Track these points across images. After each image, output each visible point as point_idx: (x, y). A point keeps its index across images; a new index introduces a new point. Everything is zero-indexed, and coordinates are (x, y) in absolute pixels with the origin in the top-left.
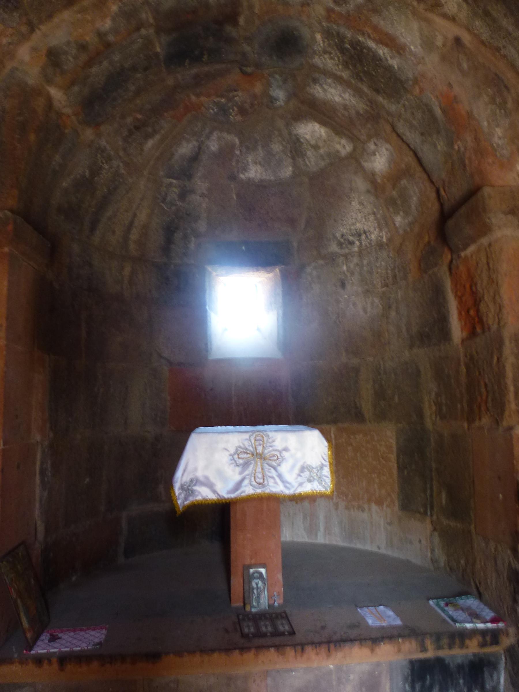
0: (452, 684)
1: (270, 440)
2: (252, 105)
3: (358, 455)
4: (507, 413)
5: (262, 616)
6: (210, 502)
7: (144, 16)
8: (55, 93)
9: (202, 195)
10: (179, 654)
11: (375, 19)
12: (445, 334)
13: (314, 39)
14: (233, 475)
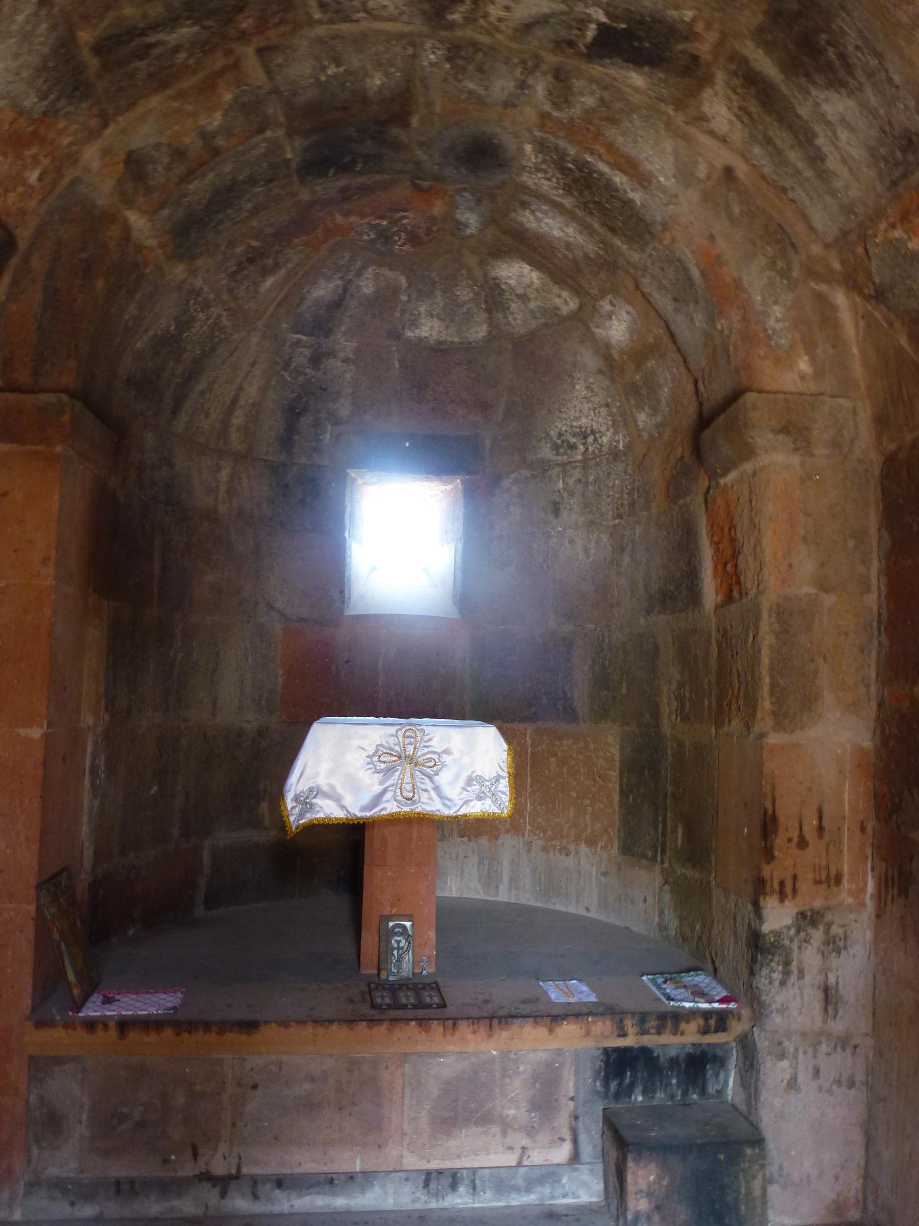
0: (661, 1084)
1: (426, 738)
2: (428, 232)
4: (759, 714)
5: (404, 985)
6: (336, 822)
7: (270, 111)
8: (136, 220)
9: (346, 361)
10: (284, 1024)
11: (611, 133)
12: (694, 597)
13: (521, 150)
14: (372, 784)
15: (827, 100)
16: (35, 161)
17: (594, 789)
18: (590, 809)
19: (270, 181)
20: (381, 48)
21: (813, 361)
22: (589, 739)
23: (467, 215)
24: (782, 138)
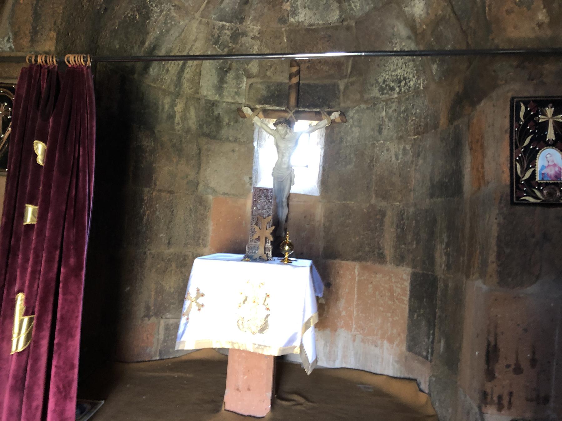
3: (377, 293)
17: (393, 307)
18: (390, 319)
21: (550, 12)
22: (392, 275)
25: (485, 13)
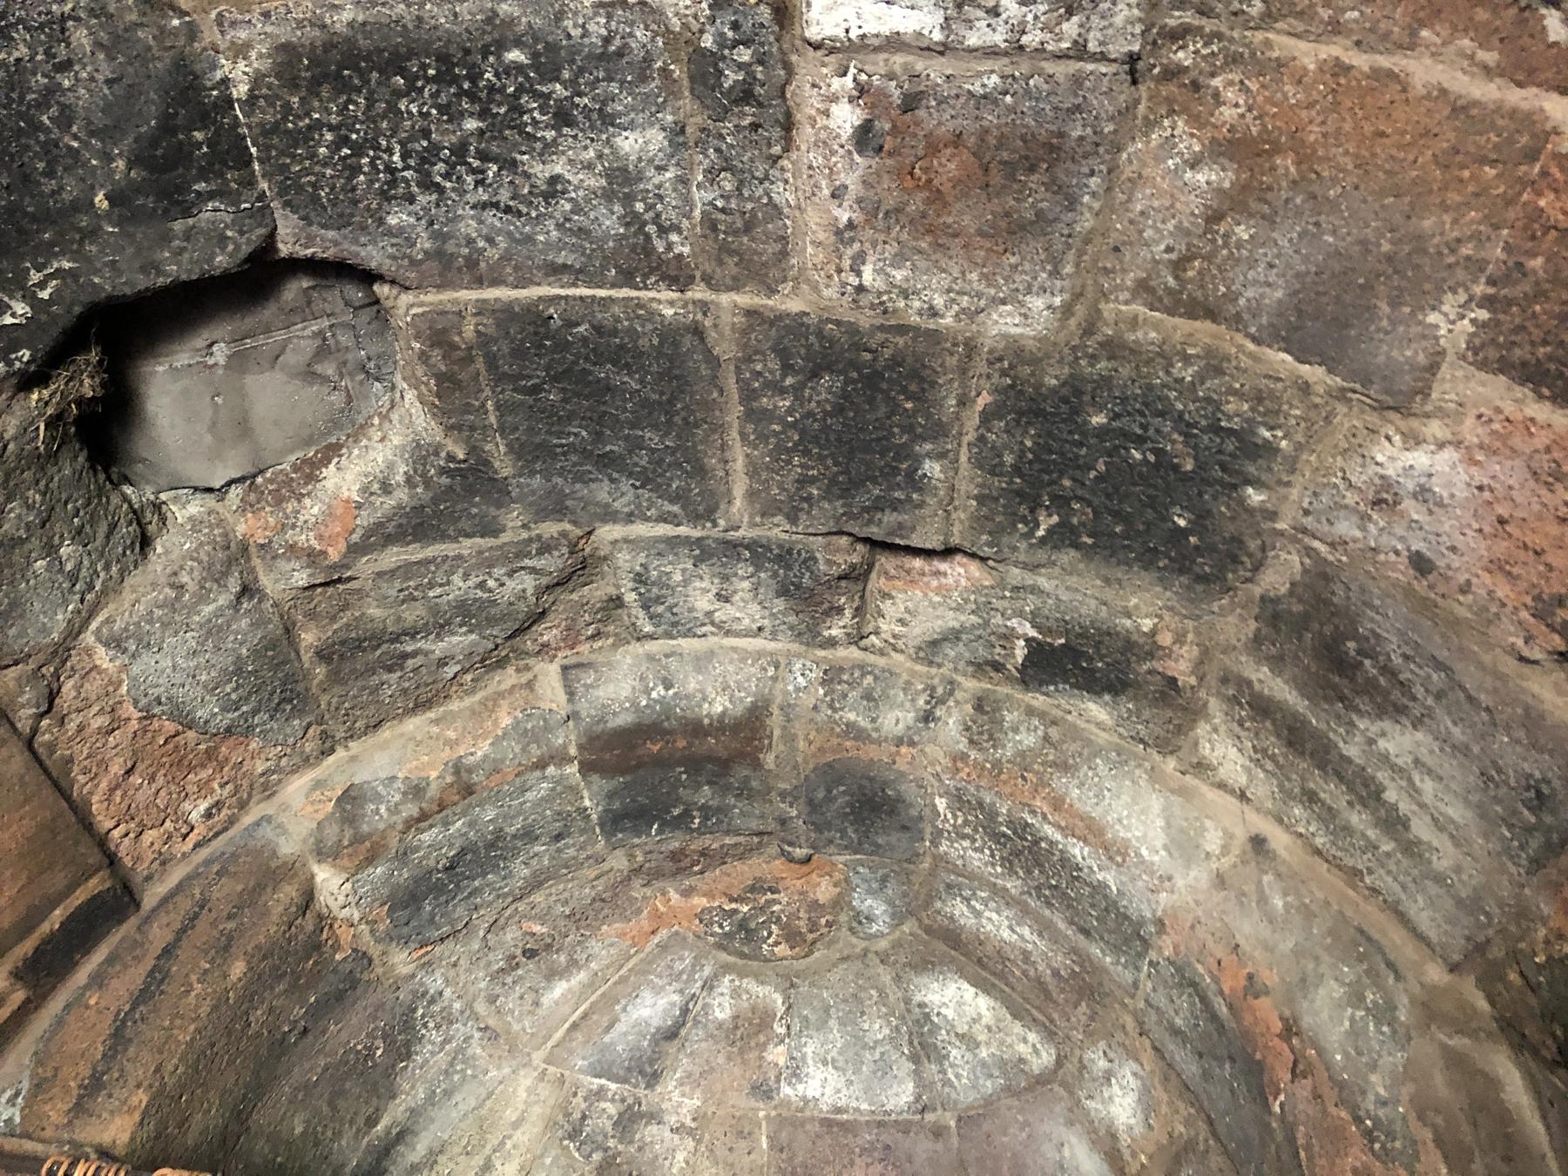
11: (1060, 782)
15: (1383, 734)
16: (204, 788)
19: (558, 837)
20: (731, 668)
23: (869, 902)
24: (1331, 792)
25: (1300, 1166)
